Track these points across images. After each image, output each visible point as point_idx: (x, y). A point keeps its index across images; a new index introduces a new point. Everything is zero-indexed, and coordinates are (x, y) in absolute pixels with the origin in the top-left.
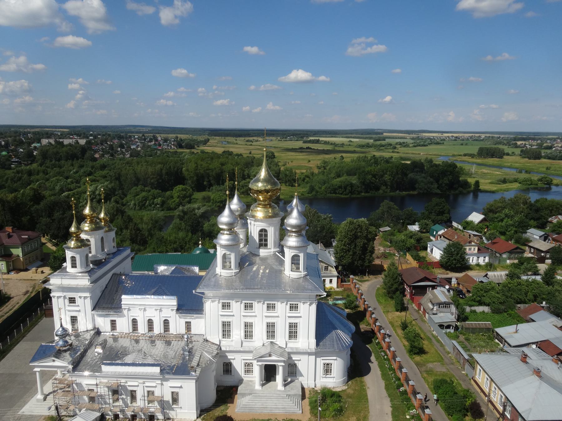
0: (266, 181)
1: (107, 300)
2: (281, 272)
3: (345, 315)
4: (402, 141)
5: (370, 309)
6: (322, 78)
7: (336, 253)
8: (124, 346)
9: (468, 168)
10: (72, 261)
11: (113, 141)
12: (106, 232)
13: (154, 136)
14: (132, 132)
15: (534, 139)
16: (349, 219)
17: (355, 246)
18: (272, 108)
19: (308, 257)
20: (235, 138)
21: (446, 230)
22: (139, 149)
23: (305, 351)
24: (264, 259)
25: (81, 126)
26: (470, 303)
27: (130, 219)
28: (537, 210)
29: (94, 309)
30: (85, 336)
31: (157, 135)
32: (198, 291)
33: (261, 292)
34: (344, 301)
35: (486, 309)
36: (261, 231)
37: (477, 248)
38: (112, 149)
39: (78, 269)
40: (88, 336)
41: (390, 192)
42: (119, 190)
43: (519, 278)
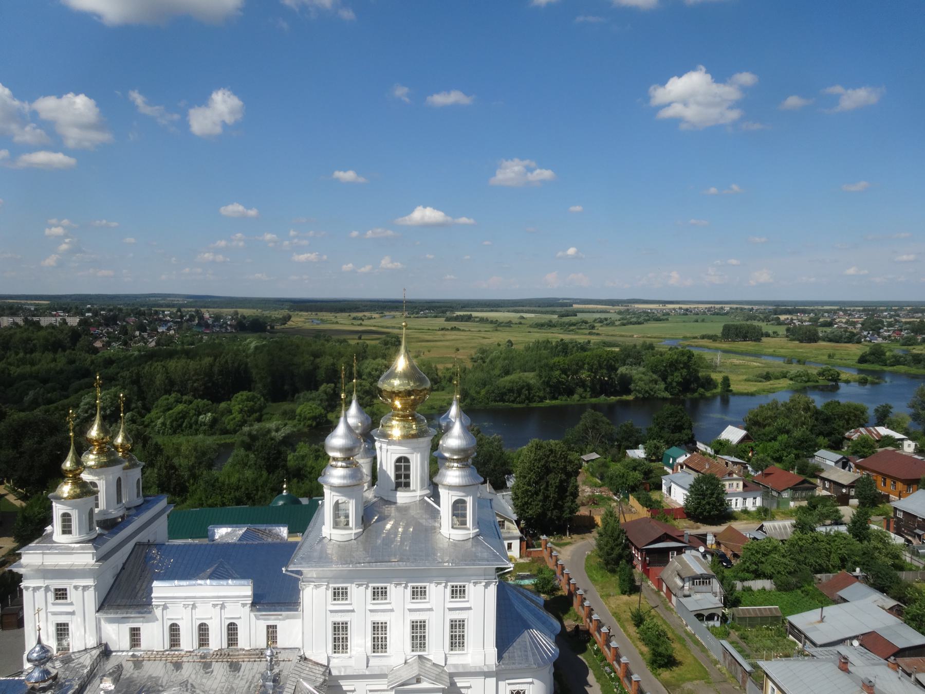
0: (406, 376)
1: (124, 592)
2: (434, 530)
3: (542, 603)
4: (603, 316)
5: (578, 592)
6: (464, 220)
7: (515, 498)
8: (154, 675)
9: (710, 357)
10: (64, 521)
11: (127, 319)
12: (125, 468)
13: (197, 312)
14: (161, 306)
15: (804, 312)
16: (534, 441)
17: (547, 486)
18: (390, 265)
19: (480, 504)
20: (333, 314)
21: (689, 455)
22: (172, 332)
23: (478, 670)
24: (404, 509)
25: (70, 296)
26: (741, 575)
27: (158, 450)
28: (827, 420)
29: (100, 609)
30: (81, 660)
31: (203, 310)
32: (292, 568)
35: (767, 584)
36: (399, 460)
37: (741, 484)
38: (126, 333)
39: (75, 536)
40: (87, 661)
41: (591, 397)
42: (138, 400)
43: (813, 530)
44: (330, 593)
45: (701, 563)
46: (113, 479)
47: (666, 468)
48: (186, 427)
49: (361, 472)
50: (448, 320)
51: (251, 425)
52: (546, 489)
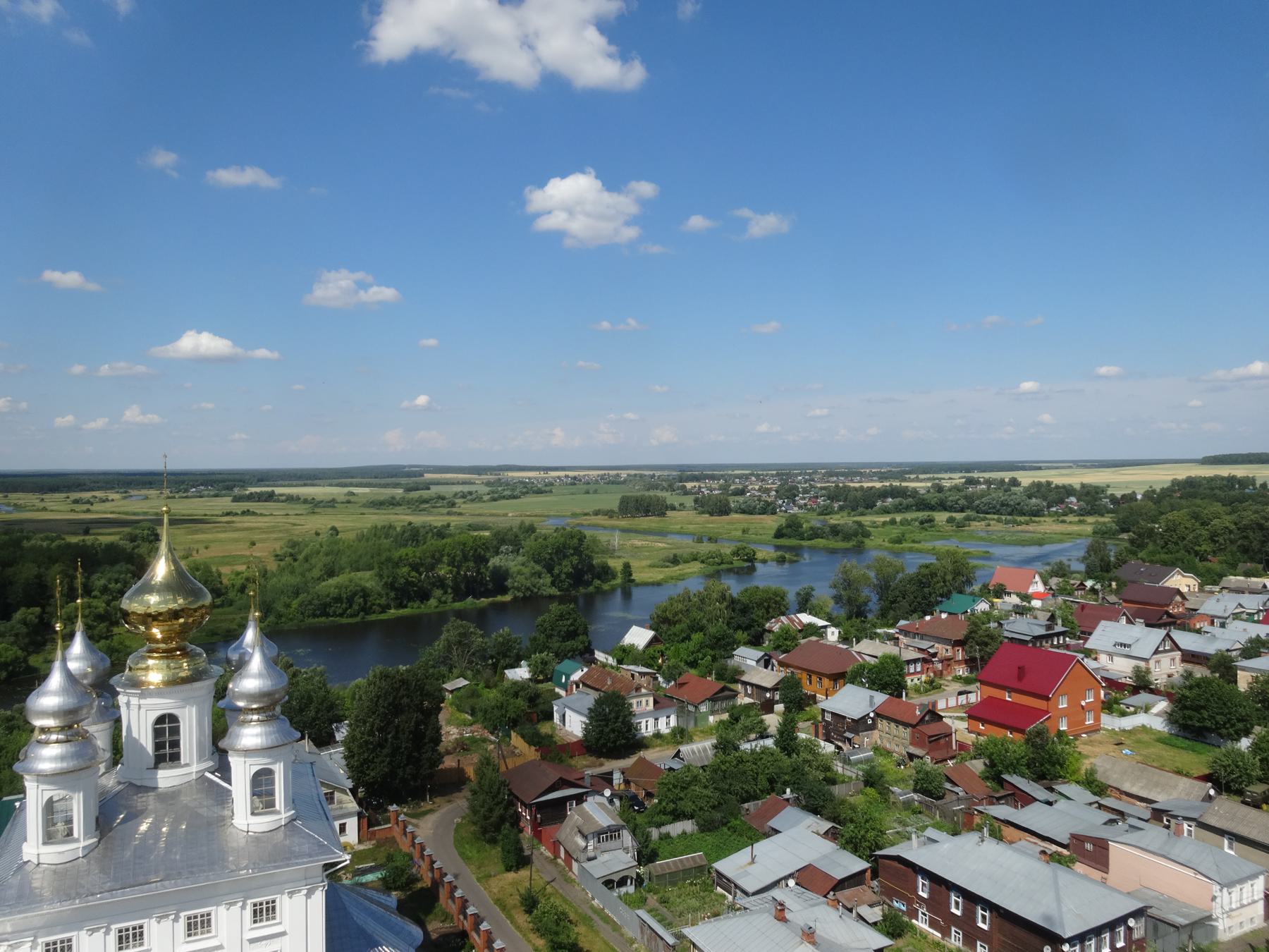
0: (172, 587)
2: (223, 821)
4: (466, 488)
6: (262, 353)
15: (712, 478)
18: (139, 419)
20: (38, 495)
21: (585, 670)
24: (171, 796)
26: (656, 819)
28: (745, 610)
33: (170, 887)
34: (379, 875)
35: (687, 826)
36: (160, 720)
37: (651, 700)
41: (454, 601)
43: (737, 748)
47: (557, 690)
49: (95, 748)
50: (237, 499)
52: (396, 737)
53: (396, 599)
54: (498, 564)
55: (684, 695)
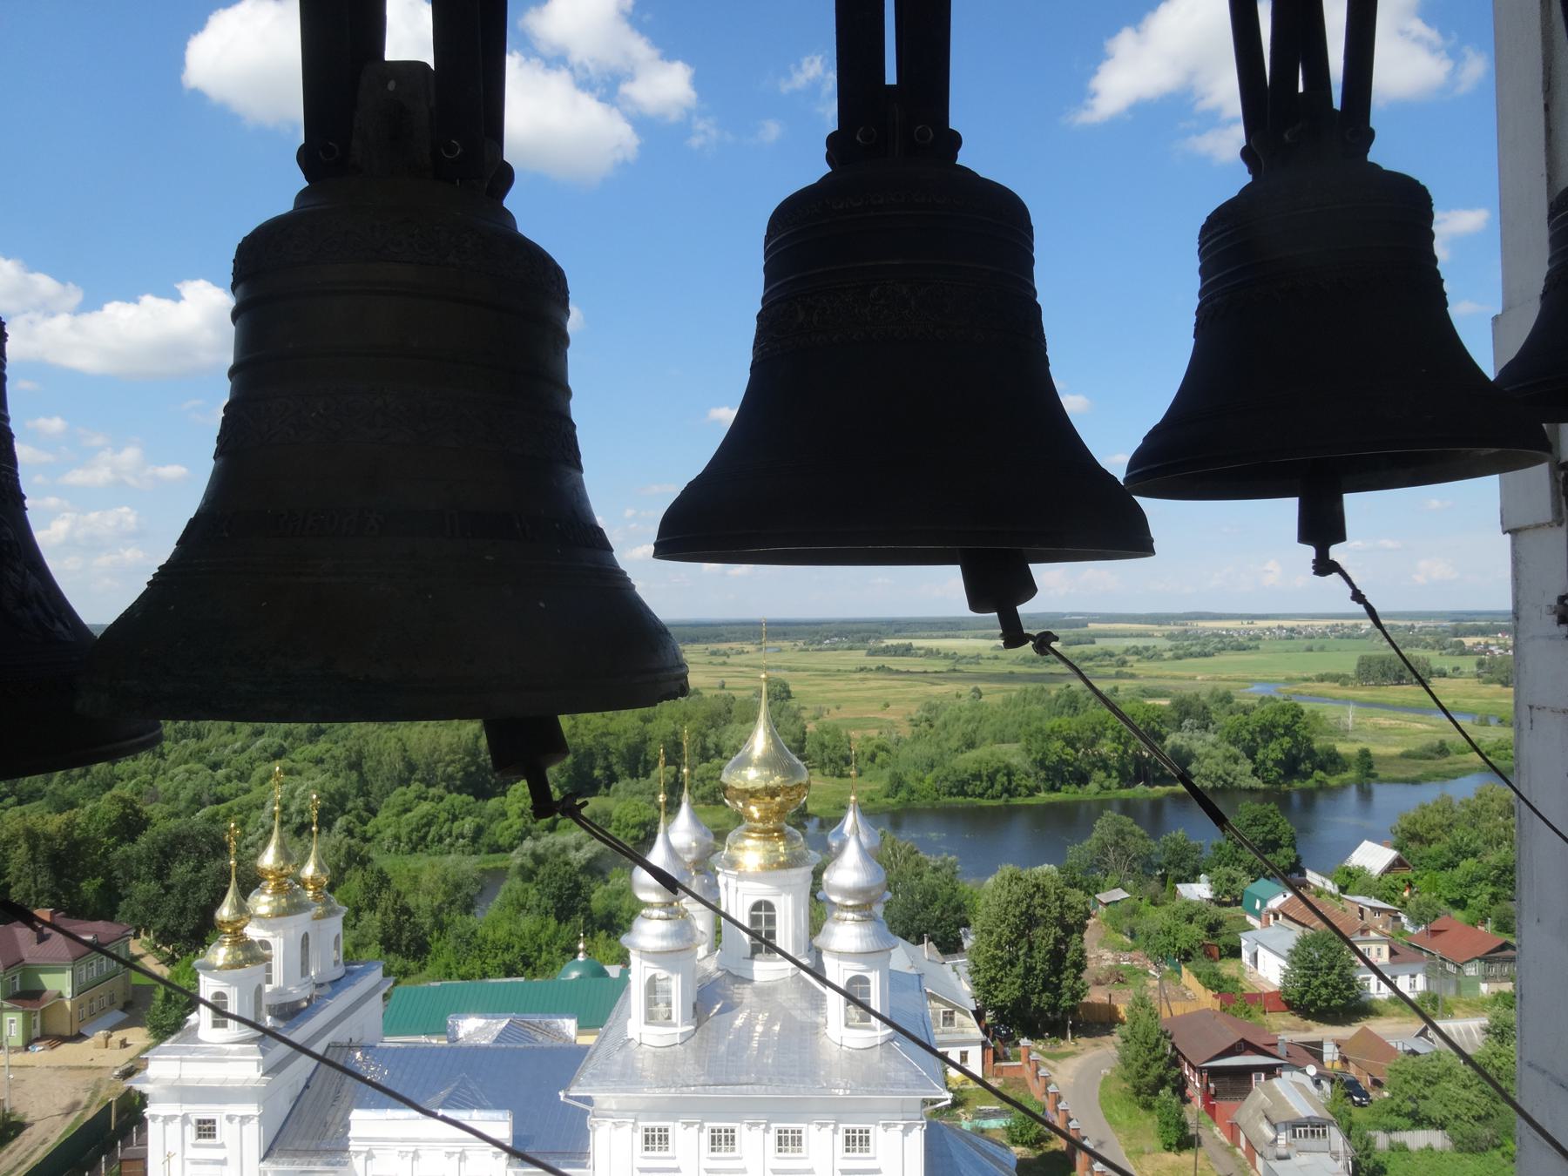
2: (815, 1029)
4: (1141, 643)
7: (975, 971)
12: (318, 917)
16: (1007, 869)
17: (1031, 948)
24: (766, 993)
26: (1385, 1119)
29: (267, 1155)
32: (575, 1091)
35: (1435, 1139)
36: (757, 906)
37: (1385, 949)
41: (1120, 787)
44: (639, 1138)
45: (1308, 1096)
46: (295, 935)
47: (1249, 918)
48: (433, 841)
49: (693, 928)
50: (873, 653)
51: (536, 838)
52: (1029, 954)
53: (1047, 780)
54: (1179, 742)
55: (1438, 947)
